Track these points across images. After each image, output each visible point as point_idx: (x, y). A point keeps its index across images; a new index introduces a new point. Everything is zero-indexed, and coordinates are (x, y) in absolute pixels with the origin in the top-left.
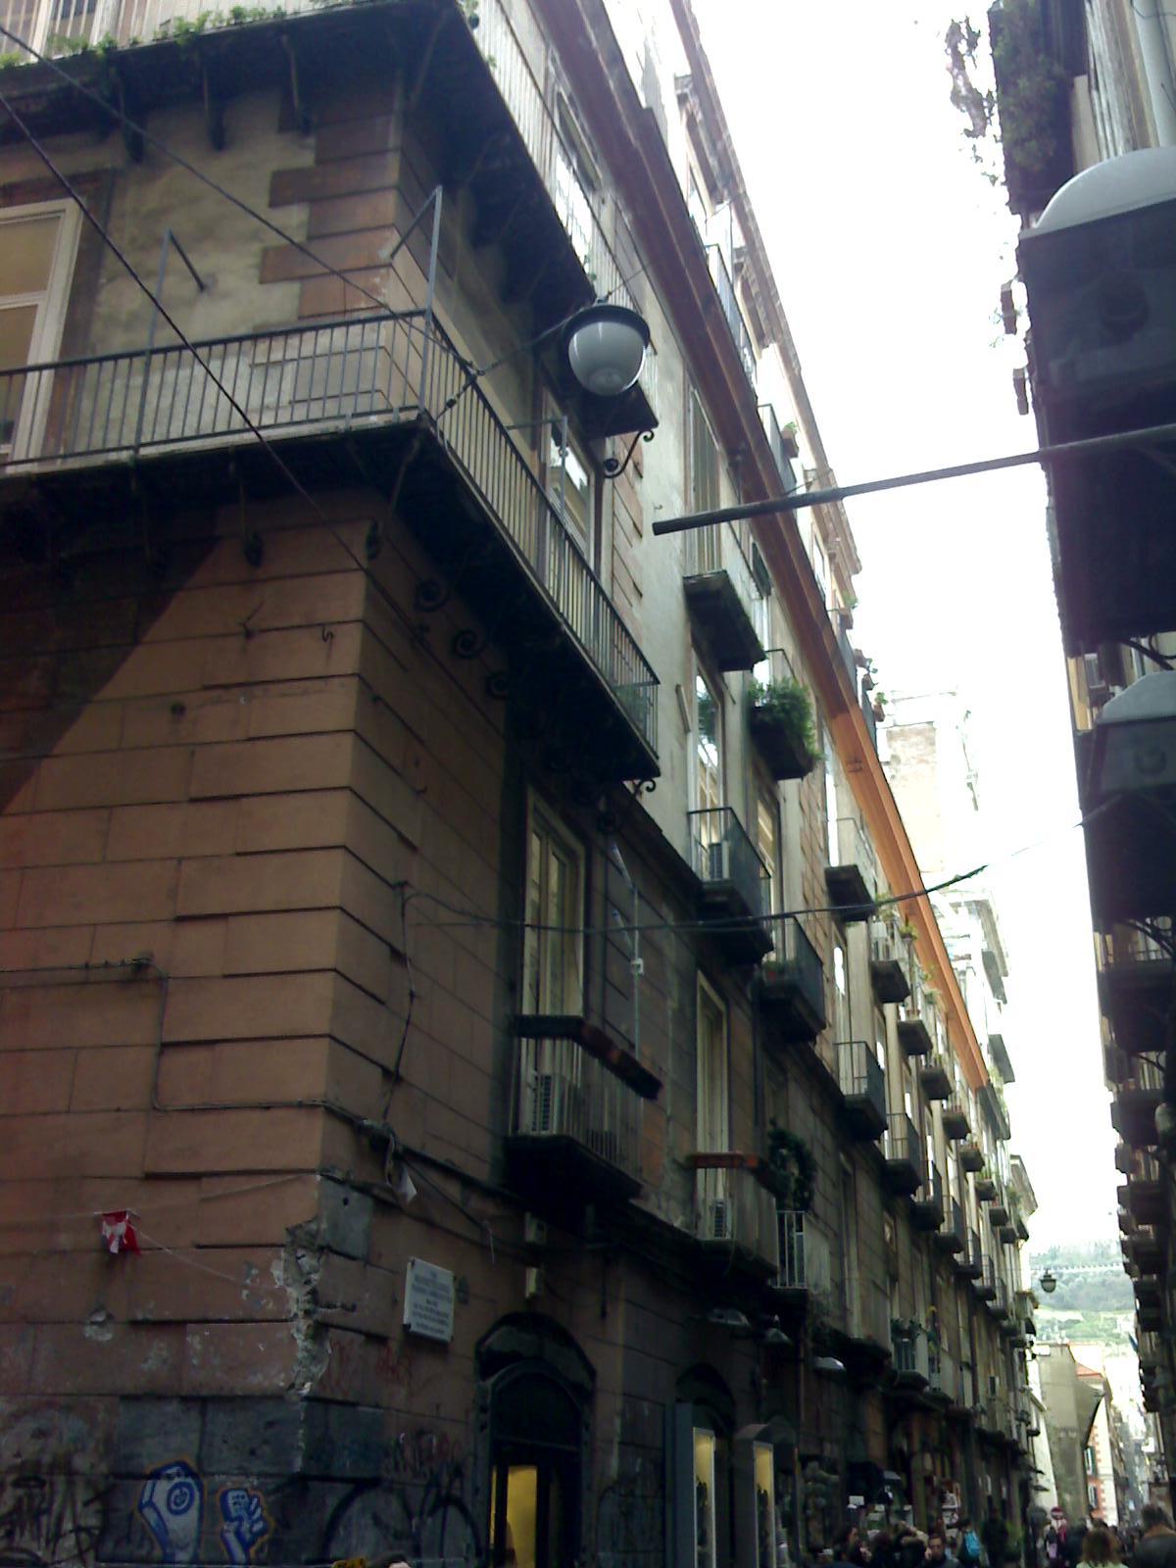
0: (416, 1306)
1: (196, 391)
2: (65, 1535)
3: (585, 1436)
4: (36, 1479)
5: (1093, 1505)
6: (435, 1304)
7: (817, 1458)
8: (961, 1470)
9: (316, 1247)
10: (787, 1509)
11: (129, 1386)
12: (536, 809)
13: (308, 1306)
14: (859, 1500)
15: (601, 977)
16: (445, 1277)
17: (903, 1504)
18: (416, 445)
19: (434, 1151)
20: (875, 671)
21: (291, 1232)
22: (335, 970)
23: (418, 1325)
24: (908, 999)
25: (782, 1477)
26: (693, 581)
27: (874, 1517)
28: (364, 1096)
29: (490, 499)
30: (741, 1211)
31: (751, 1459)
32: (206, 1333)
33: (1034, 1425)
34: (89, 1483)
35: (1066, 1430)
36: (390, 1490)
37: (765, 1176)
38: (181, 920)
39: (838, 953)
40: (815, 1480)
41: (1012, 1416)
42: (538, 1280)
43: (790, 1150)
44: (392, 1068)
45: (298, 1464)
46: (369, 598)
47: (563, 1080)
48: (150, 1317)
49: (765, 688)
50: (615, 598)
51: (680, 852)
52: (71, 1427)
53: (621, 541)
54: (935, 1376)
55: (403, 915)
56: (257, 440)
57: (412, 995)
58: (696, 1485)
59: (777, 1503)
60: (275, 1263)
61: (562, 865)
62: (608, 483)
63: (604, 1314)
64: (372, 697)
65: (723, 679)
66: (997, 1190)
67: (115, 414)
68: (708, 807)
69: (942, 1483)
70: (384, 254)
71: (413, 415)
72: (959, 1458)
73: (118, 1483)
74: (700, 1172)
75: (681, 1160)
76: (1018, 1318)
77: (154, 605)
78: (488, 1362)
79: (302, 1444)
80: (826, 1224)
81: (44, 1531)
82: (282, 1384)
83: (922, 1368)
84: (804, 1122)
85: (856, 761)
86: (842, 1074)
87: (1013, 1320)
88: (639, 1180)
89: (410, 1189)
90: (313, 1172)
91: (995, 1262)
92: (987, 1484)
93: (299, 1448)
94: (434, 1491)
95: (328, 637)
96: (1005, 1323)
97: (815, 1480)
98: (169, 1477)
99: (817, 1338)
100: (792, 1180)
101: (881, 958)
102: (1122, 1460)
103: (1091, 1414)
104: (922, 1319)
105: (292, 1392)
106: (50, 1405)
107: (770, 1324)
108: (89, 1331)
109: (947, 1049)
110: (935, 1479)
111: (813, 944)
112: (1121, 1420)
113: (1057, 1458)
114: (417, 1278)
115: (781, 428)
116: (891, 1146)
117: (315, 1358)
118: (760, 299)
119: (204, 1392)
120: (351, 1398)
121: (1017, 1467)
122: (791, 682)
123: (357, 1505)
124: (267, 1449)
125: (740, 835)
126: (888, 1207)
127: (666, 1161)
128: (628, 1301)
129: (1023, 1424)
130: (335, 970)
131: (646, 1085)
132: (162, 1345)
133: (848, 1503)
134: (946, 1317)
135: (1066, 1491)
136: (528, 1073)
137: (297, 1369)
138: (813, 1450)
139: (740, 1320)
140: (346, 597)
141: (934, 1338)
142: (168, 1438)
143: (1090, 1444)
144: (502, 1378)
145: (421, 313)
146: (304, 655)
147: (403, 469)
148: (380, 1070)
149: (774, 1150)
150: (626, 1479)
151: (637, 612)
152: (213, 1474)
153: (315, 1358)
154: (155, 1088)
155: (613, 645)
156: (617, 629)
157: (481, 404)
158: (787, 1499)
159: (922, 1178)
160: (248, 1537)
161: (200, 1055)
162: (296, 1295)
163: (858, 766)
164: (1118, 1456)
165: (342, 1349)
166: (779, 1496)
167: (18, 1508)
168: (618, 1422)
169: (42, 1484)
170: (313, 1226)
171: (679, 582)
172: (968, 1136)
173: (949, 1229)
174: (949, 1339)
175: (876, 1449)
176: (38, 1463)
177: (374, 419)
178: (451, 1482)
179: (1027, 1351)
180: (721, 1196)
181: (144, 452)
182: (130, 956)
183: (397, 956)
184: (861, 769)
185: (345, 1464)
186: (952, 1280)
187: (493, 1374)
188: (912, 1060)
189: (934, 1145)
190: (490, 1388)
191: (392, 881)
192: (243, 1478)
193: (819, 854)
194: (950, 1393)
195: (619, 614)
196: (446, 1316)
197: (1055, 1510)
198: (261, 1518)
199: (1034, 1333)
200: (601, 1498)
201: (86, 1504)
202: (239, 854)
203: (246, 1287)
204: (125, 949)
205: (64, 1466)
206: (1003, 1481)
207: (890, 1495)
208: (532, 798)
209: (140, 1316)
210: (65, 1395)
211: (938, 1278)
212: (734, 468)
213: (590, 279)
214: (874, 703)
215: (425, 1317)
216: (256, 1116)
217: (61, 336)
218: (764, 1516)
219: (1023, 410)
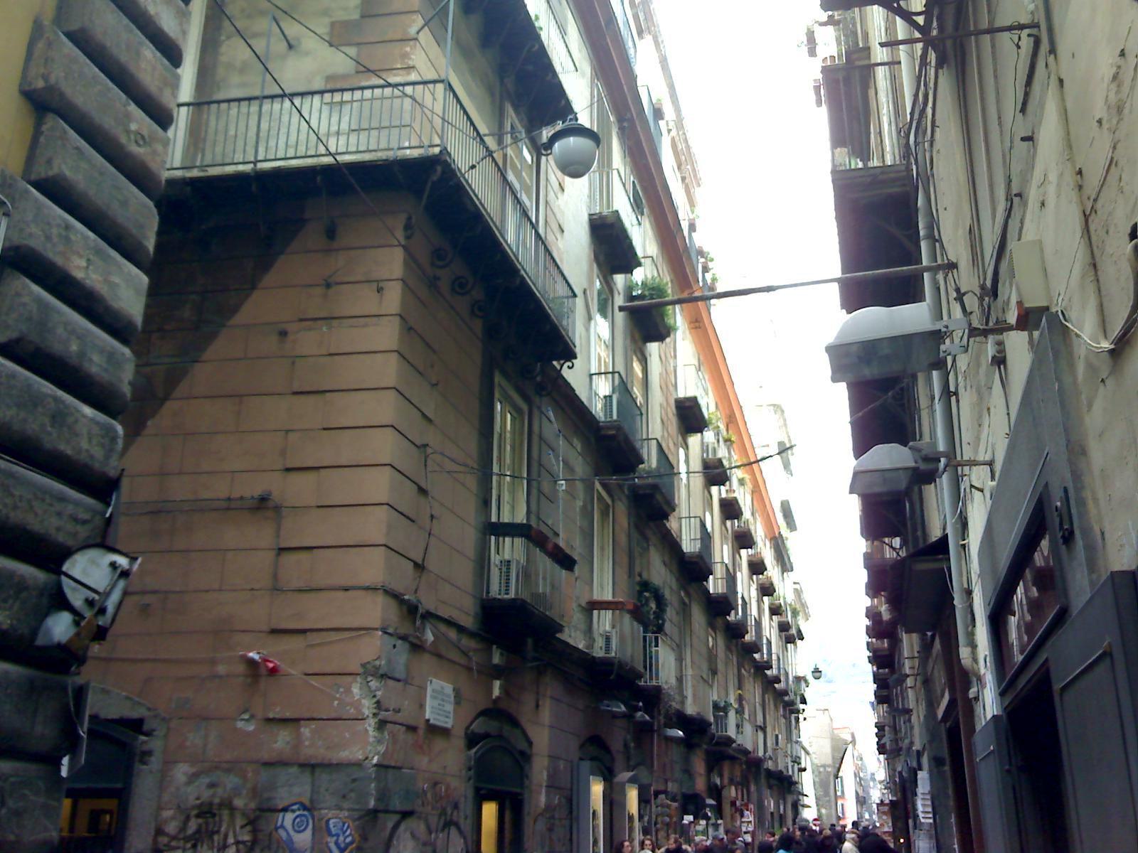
0: (432, 707)
1: (285, 118)
2: (229, 846)
3: (527, 782)
4: (210, 812)
5: (840, 815)
6: (443, 706)
7: (665, 792)
8: (754, 796)
9: (379, 675)
10: (646, 824)
11: (266, 756)
12: (500, 385)
13: (375, 711)
14: (691, 818)
15: (538, 493)
16: (449, 689)
17: (717, 819)
18: (439, 169)
19: (444, 612)
20: (712, 260)
21: (363, 665)
22: (388, 504)
23: (434, 719)
24: (728, 483)
25: (643, 805)
26: (595, 217)
27: (699, 828)
28: (404, 580)
29: (480, 197)
30: (622, 639)
31: (624, 795)
32: (347, 735)
33: (803, 766)
34: (244, 814)
35: (824, 766)
36: (419, 818)
37: (637, 614)
38: (288, 470)
39: (682, 451)
40: (662, 806)
41: (789, 760)
42: (501, 688)
43: (651, 593)
44: (420, 562)
45: (372, 803)
46: (406, 263)
47: (518, 562)
48: (277, 716)
49: (640, 283)
50: (548, 238)
51: (586, 403)
52: (231, 781)
53: (551, 195)
54: (740, 736)
55: (426, 465)
56: (335, 162)
57: (432, 517)
58: (591, 811)
59: (639, 821)
60: (354, 685)
61: (513, 419)
62: (544, 158)
63: (537, 706)
64: (408, 329)
65: (612, 279)
66: (784, 608)
67: (232, 132)
68: (603, 371)
69: (742, 805)
70: (412, 31)
71: (437, 150)
72: (753, 788)
73: (262, 814)
74: (595, 612)
75: (584, 604)
76: (796, 695)
77: (265, 264)
78: (472, 740)
79: (374, 792)
80: (671, 638)
81: (216, 844)
82: (360, 757)
83: (732, 732)
84: (660, 573)
85: (697, 321)
86: (684, 537)
87: (792, 696)
88: (561, 623)
89: (430, 637)
90: (376, 629)
91: (781, 658)
92: (771, 804)
93: (372, 794)
94: (443, 818)
95: (380, 290)
96: (786, 698)
97: (662, 806)
98: (293, 811)
99: (668, 716)
100: (652, 612)
101: (710, 456)
102: (861, 785)
103: (841, 755)
104: (732, 699)
105: (367, 761)
106: (217, 768)
107: (637, 709)
108: (240, 724)
109: (753, 514)
110: (738, 803)
111: (666, 451)
112: (861, 759)
113: (817, 785)
114: (433, 691)
115: (654, 102)
116: (715, 585)
117: (379, 742)
118: (641, 7)
119: (313, 762)
120: (398, 764)
121: (790, 792)
122: (657, 280)
123: (402, 827)
124: (353, 795)
125: (623, 388)
126: (711, 625)
127: (574, 606)
128: (552, 697)
129: (796, 765)
130: (388, 504)
131: (566, 562)
132: (285, 733)
133: (683, 819)
134: (747, 696)
135: (822, 806)
136: (495, 559)
137: (369, 748)
138: (662, 788)
139: (620, 708)
140: (391, 263)
141: (740, 712)
142: (293, 788)
143: (840, 774)
144: (481, 748)
145: (442, 81)
146: (366, 301)
147: (429, 184)
148: (412, 563)
149: (640, 593)
150: (549, 807)
151: (561, 244)
152: (320, 809)
153: (379, 742)
154: (275, 576)
155: (545, 268)
156: (548, 258)
157: (465, 117)
158: (646, 819)
159: (734, 606)
160: (343, 845)
161: (303, 556)
162: (367, 707)
163: (697, 324)
164: (860, 782)
165: (393, 736)
166: (641, 817)
167: (198, 831)
168: (545, 774)
169: (214, 815)
170: (377, 663)
171: (586, 218)
172: (765, 573)
173: (751, 636)
174: (749, 711)
175: (700, 785)
176: (211, 804)
177: (408, 152)
178: (452, 813)
179: (800, 715)
180: (608, 628)
181: (261, 166)
182: (257, 491)
183: (422, 491)
184: (700, 328)
185: (397, 804)
186: (752, 671)
187: (474, 747)
188: (729, 523)
189: (742, 576)
190: (473, 755)
191: (418, 442)
192: (338, 812)
193: (671, 388)
194: (749, 747)
195: (550, 248)
196: (449, 713)
197: (815, 820)
198: (350, 835)
199: (806, 703)
200: (535, 821)
201: (242, 827)
202: (324, 429)
203: (337, 699)
204: (253, 488)
205: (228, 804)
206: (781, 801)
207: (709, 814)
208: (498, 378)
209: (271, 715)
210: (225, 762)
211: (743, 671)
212: (622, 129)
213: (538, 30)
214: (709, 281)
215: (439, 714)
216: (341, 594)
217: (196, 75)
218: (631, 829)
219: (819, 103)
